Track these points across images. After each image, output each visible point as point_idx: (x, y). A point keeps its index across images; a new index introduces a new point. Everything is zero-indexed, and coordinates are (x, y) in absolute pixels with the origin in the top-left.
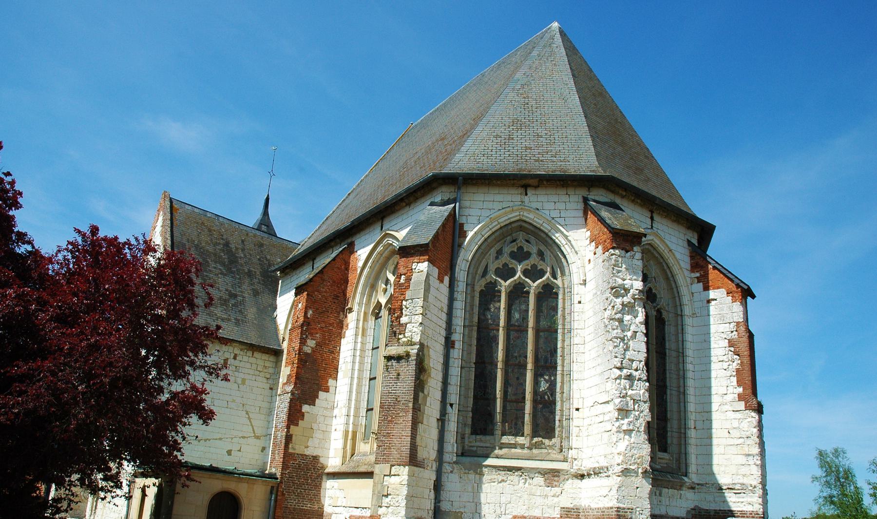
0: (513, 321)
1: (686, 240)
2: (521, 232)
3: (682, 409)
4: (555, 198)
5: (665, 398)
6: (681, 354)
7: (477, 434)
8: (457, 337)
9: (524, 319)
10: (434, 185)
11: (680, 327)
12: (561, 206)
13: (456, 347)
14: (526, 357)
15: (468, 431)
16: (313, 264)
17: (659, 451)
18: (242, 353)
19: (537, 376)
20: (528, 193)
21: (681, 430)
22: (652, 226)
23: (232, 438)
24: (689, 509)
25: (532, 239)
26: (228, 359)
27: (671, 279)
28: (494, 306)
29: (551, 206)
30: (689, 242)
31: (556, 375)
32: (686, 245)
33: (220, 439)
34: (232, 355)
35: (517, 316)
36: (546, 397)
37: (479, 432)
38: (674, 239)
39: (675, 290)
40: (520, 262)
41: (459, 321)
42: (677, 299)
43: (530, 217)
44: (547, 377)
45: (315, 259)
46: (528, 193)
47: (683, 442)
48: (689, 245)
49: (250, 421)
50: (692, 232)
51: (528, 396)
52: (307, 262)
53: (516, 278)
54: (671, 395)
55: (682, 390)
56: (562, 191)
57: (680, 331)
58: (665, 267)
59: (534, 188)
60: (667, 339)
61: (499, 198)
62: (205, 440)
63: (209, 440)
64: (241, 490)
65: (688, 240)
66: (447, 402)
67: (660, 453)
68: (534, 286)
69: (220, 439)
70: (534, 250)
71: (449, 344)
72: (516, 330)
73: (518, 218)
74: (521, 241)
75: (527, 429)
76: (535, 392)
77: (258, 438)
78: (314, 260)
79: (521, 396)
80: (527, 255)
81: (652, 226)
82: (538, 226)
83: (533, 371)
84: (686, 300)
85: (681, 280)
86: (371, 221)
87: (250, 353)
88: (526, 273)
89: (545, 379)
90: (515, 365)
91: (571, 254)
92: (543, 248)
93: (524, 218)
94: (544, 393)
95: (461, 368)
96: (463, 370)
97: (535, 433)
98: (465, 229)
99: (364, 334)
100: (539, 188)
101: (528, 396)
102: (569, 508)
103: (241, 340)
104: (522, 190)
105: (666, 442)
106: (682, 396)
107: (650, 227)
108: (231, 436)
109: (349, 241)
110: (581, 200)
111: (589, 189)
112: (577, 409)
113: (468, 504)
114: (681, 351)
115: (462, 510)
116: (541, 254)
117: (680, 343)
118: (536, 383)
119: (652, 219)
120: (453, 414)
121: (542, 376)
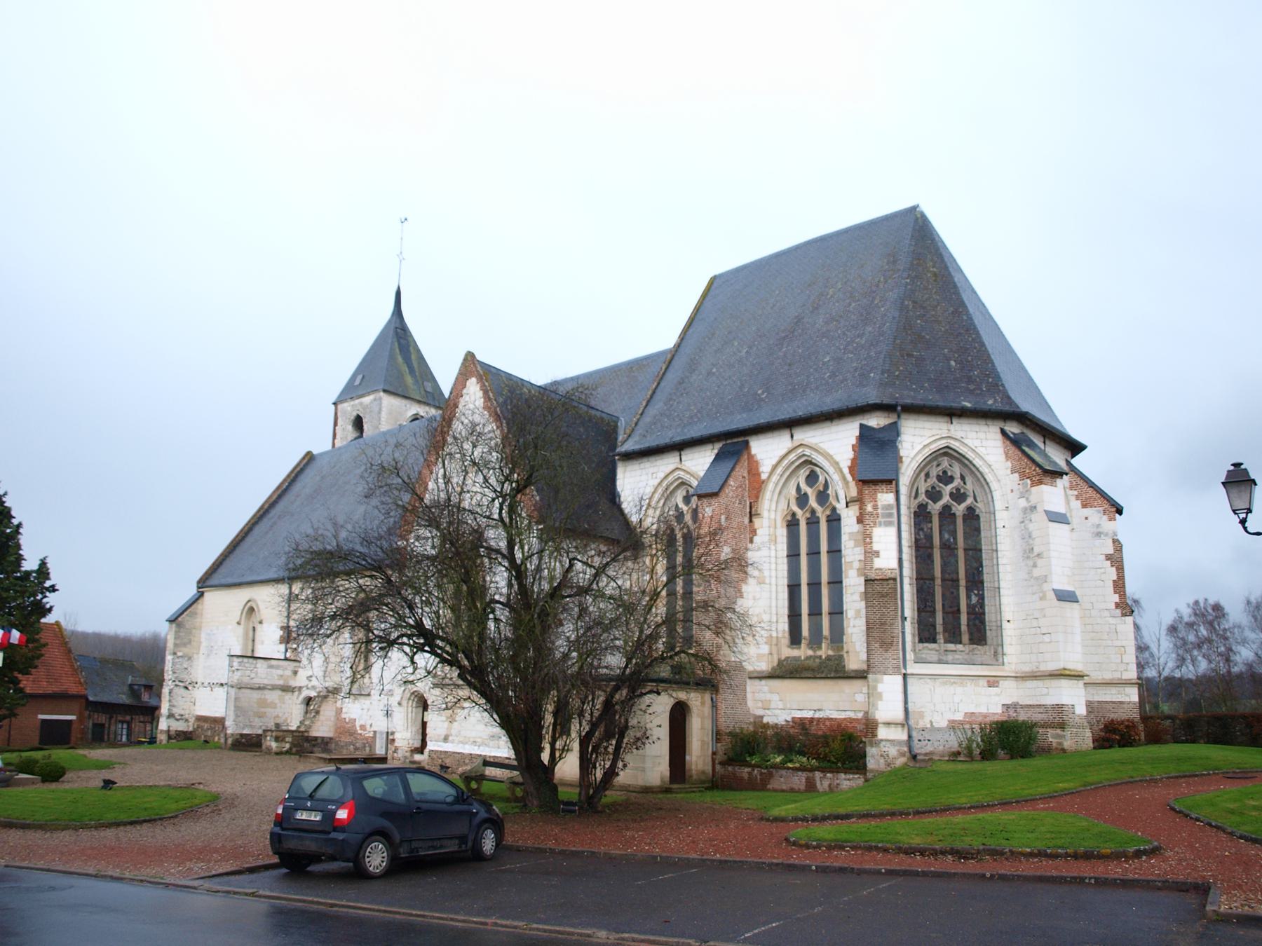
0: (944, 540)
2: (946, 458)
4: (976, 428)
7: (923, 642)
12: (982, 435)
14: (958, 573)
19: (969, 590)
20: (953, 421)
29: (973, 435)
40: (946, 485)
43: (955, 445)
50: (984, 423)
54: (260, 584)
56: (982, 422)
68: (959, 509)
72: (948, 548)
75: (965, 638)
76: (968, 606)
79: (956, 608)
80: (951, 479)
83: (915, 585)
90: (951, 582)
91: (994, 483)
92: (966, 473)
94: (975, 606)
97: (973, 641)
115: (923, 710)
116: (963, 478)
118: (969, 597)
119: (1044, 443)
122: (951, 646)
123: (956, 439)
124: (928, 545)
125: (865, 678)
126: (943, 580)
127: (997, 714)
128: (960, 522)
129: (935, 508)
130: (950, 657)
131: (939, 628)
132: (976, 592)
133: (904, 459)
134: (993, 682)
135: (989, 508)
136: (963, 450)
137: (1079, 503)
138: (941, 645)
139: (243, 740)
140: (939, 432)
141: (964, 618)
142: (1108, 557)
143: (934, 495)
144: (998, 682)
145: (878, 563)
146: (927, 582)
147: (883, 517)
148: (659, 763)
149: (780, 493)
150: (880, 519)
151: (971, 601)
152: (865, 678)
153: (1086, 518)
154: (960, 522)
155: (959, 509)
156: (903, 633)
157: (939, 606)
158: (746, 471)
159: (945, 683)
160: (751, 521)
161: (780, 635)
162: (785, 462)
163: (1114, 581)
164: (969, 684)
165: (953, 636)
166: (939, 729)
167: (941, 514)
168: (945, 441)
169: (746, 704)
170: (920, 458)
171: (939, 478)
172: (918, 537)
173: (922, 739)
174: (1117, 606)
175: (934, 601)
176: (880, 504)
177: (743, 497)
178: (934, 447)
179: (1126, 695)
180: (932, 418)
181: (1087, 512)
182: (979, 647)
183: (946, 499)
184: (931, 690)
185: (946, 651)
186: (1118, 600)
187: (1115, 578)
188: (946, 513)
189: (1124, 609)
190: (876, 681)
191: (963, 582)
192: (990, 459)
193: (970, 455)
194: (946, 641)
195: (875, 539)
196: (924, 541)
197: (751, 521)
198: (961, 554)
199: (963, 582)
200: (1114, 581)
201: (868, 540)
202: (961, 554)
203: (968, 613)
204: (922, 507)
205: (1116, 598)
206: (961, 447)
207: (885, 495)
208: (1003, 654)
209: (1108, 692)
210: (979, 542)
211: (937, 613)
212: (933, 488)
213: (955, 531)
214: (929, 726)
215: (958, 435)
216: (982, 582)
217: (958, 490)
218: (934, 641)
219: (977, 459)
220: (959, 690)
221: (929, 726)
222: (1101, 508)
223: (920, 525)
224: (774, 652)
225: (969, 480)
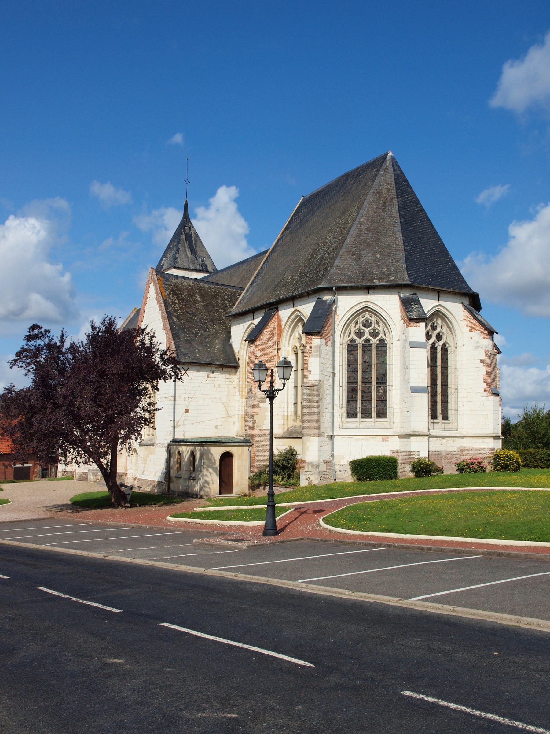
2: (367, 313)
8: (337, 371)
18: (216, 370)
33: (211, 420)
40: (368, 328)
62: (203, 422)
63: (205, 421)
64: (233, 450)
67: (235, 490)
68: (374, 341)
69: (211, 420)
72: (367, 365)
87: (221, 369)
90: (367, 381)
93: (368, 306)
97: (379, 416)
118: (378, 391)
129: (360, 342)
131: (359, 410)
137: (468, 329)
138: (374, 419)
139: (84, 476)
143: (360, 334)
149: (291, 336)
152: (301, 438)
155: (374, 341)
156: (333, 414)
158: (276, 324)
161: (289, 414)
162: (291, 319)
163: (484, 375)
165: (367, 414)
167: (378, 346)
168: (364, 304)
172: (349, 359)
176: (313, 345)
177: (273, 339)
181: (473, 334)
183: (367, 336)
186: (485, 387)
188: (367, 345)
191: (374, 383)
194: (362, 417)
197: (278, 352)
200: (484, 375)
204: (353, 341)
207: (316, 340)
210: (386, 360)
217: (374, 330)
224: (286, 423)
225: (381, 324)
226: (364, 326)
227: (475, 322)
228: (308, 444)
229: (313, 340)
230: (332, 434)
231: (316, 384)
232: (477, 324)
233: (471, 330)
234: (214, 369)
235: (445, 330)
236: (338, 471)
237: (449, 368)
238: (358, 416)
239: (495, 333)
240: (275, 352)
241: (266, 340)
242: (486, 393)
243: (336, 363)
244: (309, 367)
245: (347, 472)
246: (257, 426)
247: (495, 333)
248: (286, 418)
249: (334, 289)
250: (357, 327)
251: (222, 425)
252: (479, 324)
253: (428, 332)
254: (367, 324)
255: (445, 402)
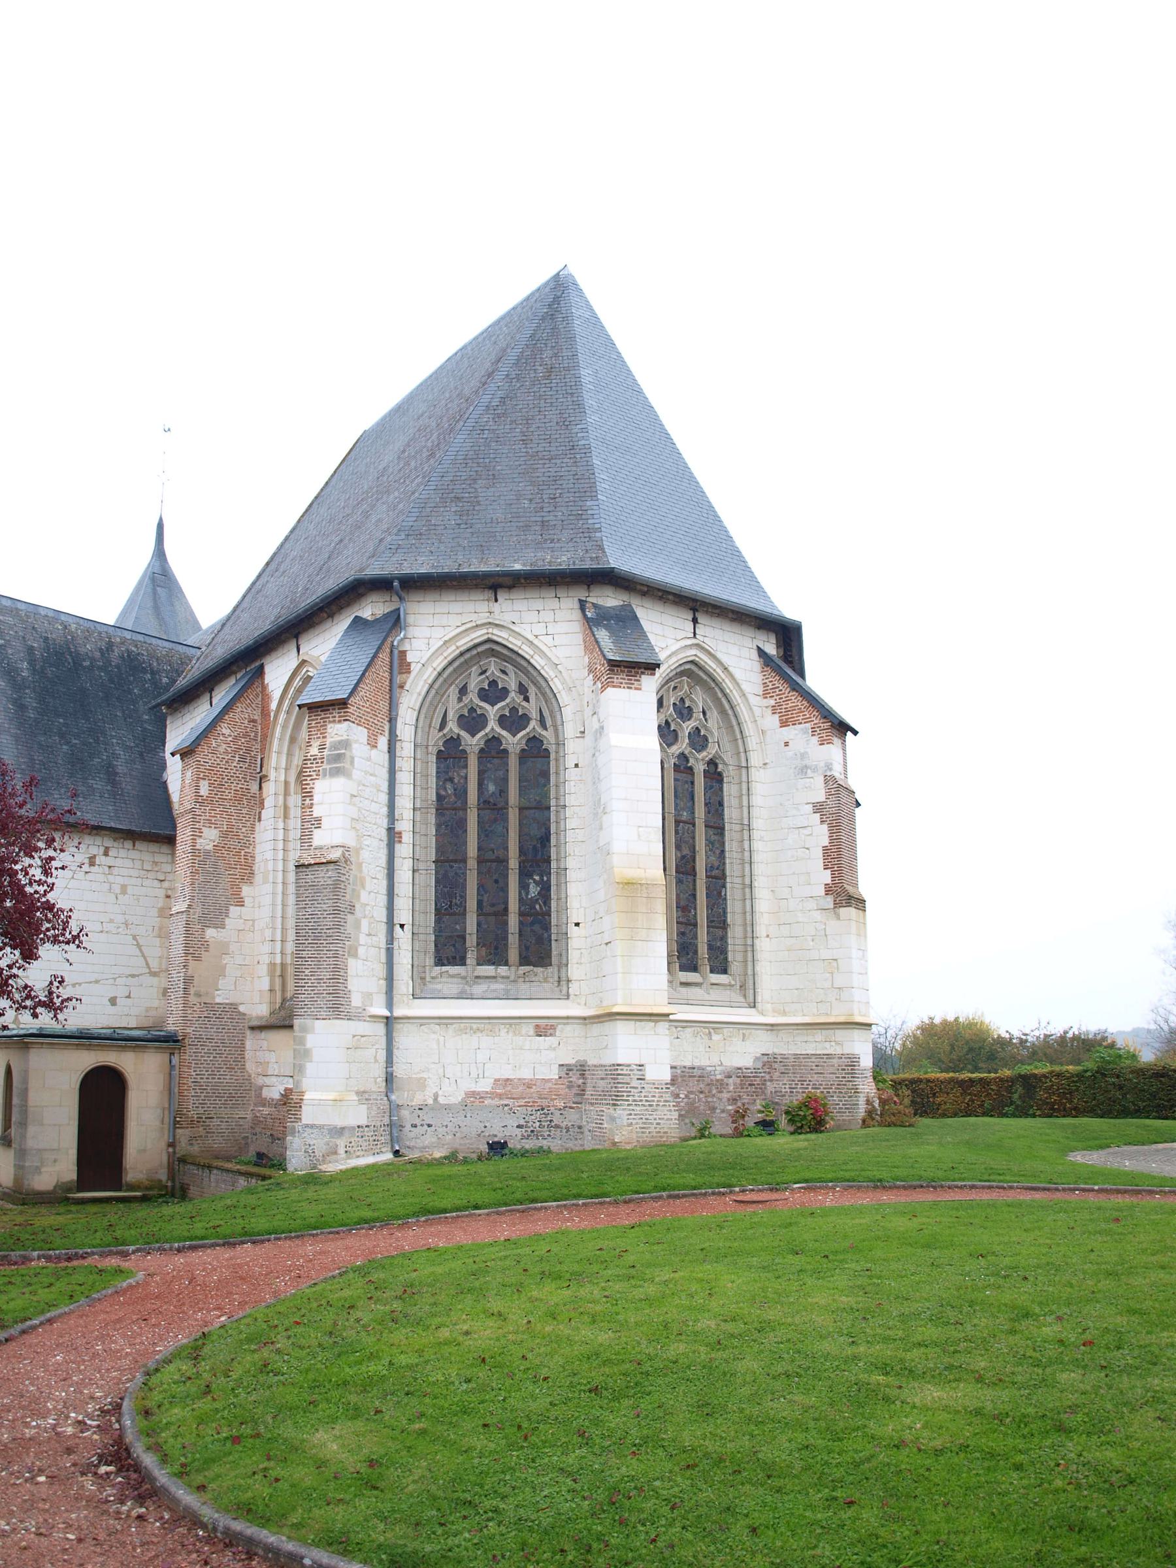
1: (755, 647)
2: (493, 659)
3: (748, 908)
4: (538, 604)
5: (723, 894)
6: (746, 827)
7: (443, 965)
8: (404, 825)
9: (501, 791)
10: (361, 591)
11: (744, 786)
12: (547, 616)
13: (404, 840)
14: (506, 849)
15: (430, 960)
16: (211, 698)
17: (712, 971)
18: (116, 844)
19: (524, 874)
21: (746, 941)
22: (695, 634)
23: (115, 979)
24: (758, 1055)
25: (510, 668)
26: (95, 856)
27: (730, 712)
28: (458, 775)
30: (761, 652)
31: (550, 874)
32: (754, 654)
33: (97, 982)
34: (102, 849)
35: (492, 788)
36: (537, 907)
37: (446, 962)
38: (734, 650)
39: (736, 728)
41: (404, 805)
42: (740, 742)
43: (501, 635)
44: (537, 878)
45: (213, 690)
46: (498, 597)
47: (750, 958)
48: (760, 656)
49: (141, 950)
51: (513, 905)
52: (202, 693)
53: (488, 730)
55: (747, 881)
57: (744, 792)
58: (720, 695)
59: (506, 590)
60: (726, 804)
61: (456, 607)
63: (80, 984)
64: (125, 1061)
65: (759, 648)
66: (395, 922)
67: (712, 975)
68: (513, 742)
69: (97, 982)
70: (513, 686)
71: (393, 836)
72: (493, 808)
73: (485, 637)
74: (493, 672)
75: (513, 954)
77: (154, 974)
78: (211, 691)
81: (695, 634)
82: (516, 649)
84: (752, 743)
85: (745, 713)
86: (283, 638)
87: (128, 844)
88: (502, 720)
89: (535, 881)
90: (493, 863)
93: (495, 638)
95: (414, 871)
96: (417, 874)
97: (524, 960)
98: (408, 660)
99: (286, 816)
100: (514, 590)
101: (513, 905)
102: (570, 1065)
103: (113, 825)
104: (491, 594)
105: (726, 959)
106: (747, 890)
107: (692, 635)
108: (112, 976)
109: (257, 664)
110: (577, 605)
111: (589, 588)
112: (577, 924)
113: (433, 1066)
114: (746, 822)
115: (425, 1075)
116: (523, 690)
117: (745, 810)
118: (524, 886)
119: (695, 621)
120: (403, 938)
121: (530, 876)
122: (489, 970)
123: (503, 626)
124: (459, 804)
125: (291, 1027)
126: (480, 861)
127: (549, 1080)
128: (513, 762)
129: (473, 743)
130: (479, 989)
131: (471, 940)
132: (537, 878)
133: (413, 666)
134: (544, 1028)
135: (739, 760)
136: (514, 643)
140: (474, 617)
141: (513, 921)
142: (818, 808)
143: (472, 722)
144: (553, 1027)
145: (320, 838)
146: (456, 865)
147: (329, 762)
148: (55, 1161)
150: (325, 766)
151: (527, 893)
153: (786, 744)
154: (513, 762)
155: (513, 742)
157: (472, 904)
159: (463, 1031)
160: (260, 788)
164: (503, 1031)
165: (494, 953)
166: (447, 1107)
167: (524, 756)
169: (243, 1068)
170: (440, 663)
171: (484, 695)
172: (443, 793)
173: (418, 1122)
174: (828, 890)
175: (464, 897)
176: (329, 741)
177: (248, 751)
178: (464, 642)
179: (837, 1043)
180: (464, 596)
181: (791, 733)
182: (539, 970)
183: (492, 725)
184: (438, 1042)
185: (477, 977)
186: (829, 881)
187: (826, 842)
188: (493, 750)
189: (838, 894)
190: (304, 1029)
191: (513, 864)
192: (557, 655)
193: (526, 651)
195: (317, 798)
196: (453, 798)
198: (513, 816)
199: (513, 864)
200: (825, 849)
201: (308, 802)
202: (513, 816)
203: (521, 914)
204: (453, 743)
205: (827, 877)
206: (511, 639)
207: (338, 726)
208: (568, 981)
209: (810, 1038)
211: (468, 916)
212: (472, 710)
213: (506, 780)
214: (430, 1102)
215: (498, 618)
216: (548, 861)
218: (463, 963)
219: (536, 657)
220: (485, 1041)
221: (430, 1102)
222: (808, 725)
223: (447, 773)
225: (532, 692)
226: (484, 695)
227: (795, 700)
228: (311, 1041)
229: (329, 726)
230: (388, 1014)
231: (335, 855)
232: (802, 704)
233: (784, 724)
234: (108, 843)
235: (714, 722)
236: (408, 1127)
237: (727, 827)
238: (468, 961)
239: (849, 733)
240: (254, 787)
241: (226, 752)
242: (830, 899)
243: (399, 802)
244: (315, 808)
245: (433, 1128)
246: (198, 995)
247: (849, 733)
248: (278, 973)
249: (396, 584)
250: (466, 700)
251: (129, 997)
252: (805, 703)
253: (667, 723)
254: (493, 693)
255: (719, 923)
